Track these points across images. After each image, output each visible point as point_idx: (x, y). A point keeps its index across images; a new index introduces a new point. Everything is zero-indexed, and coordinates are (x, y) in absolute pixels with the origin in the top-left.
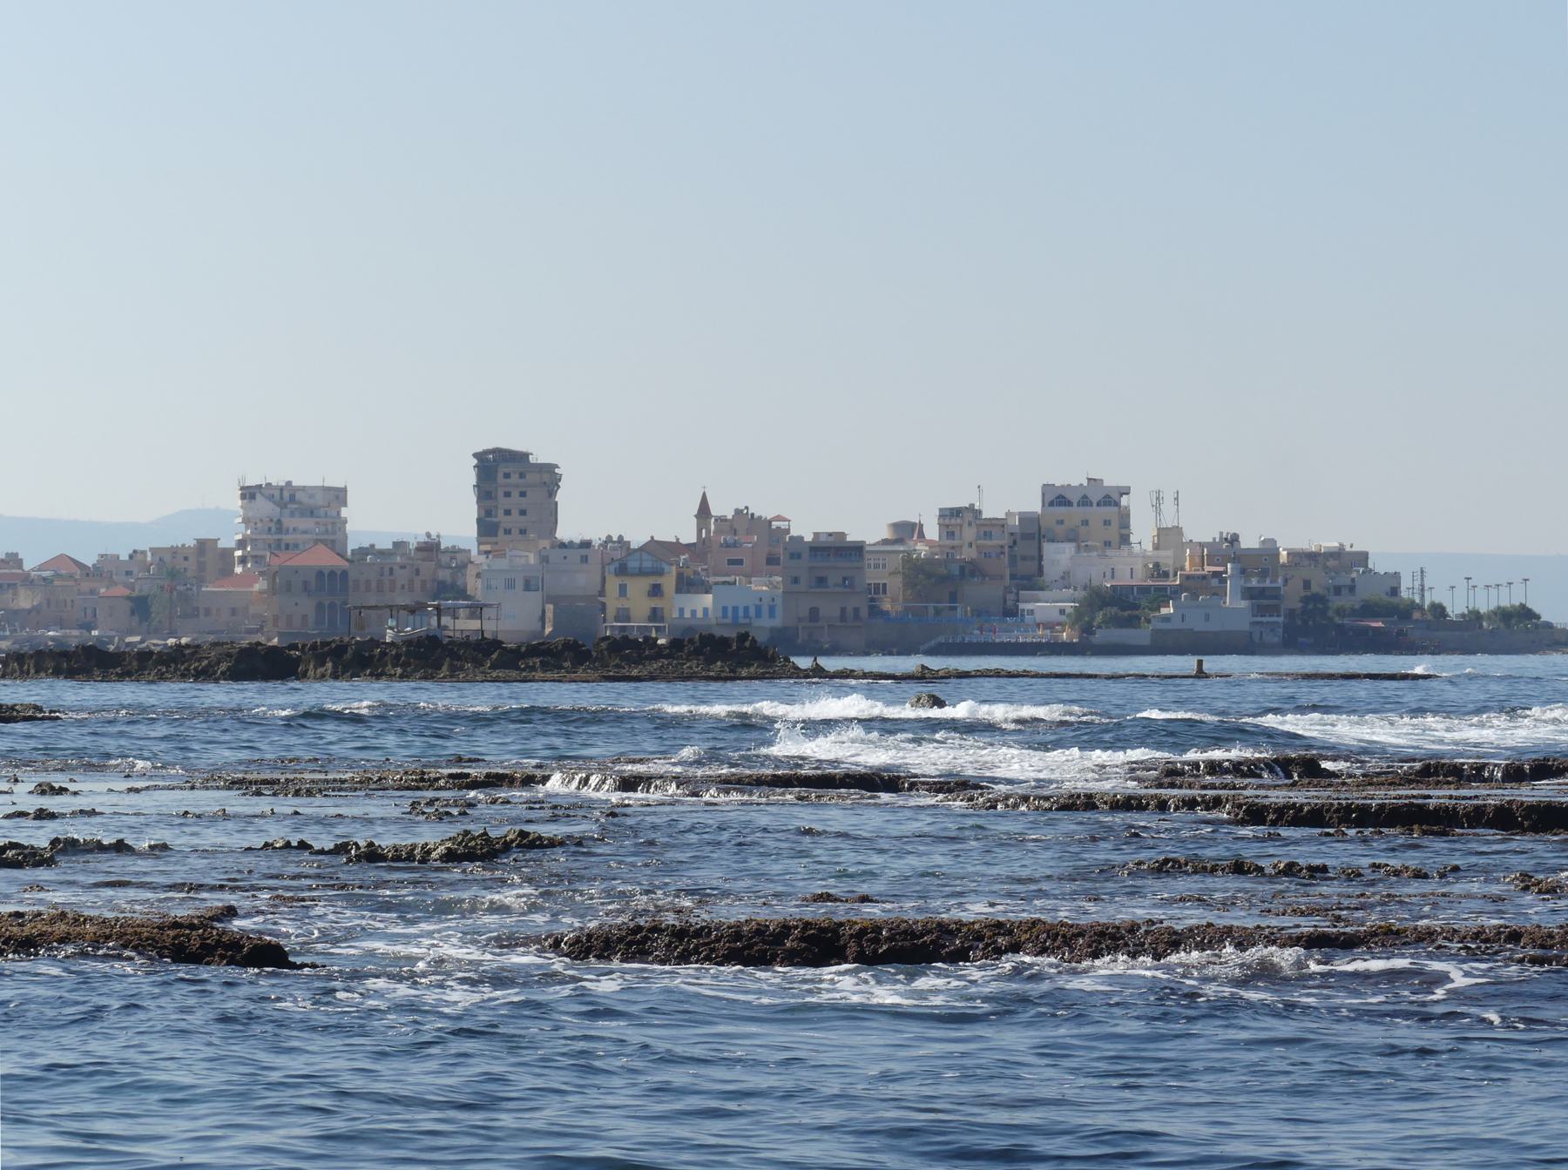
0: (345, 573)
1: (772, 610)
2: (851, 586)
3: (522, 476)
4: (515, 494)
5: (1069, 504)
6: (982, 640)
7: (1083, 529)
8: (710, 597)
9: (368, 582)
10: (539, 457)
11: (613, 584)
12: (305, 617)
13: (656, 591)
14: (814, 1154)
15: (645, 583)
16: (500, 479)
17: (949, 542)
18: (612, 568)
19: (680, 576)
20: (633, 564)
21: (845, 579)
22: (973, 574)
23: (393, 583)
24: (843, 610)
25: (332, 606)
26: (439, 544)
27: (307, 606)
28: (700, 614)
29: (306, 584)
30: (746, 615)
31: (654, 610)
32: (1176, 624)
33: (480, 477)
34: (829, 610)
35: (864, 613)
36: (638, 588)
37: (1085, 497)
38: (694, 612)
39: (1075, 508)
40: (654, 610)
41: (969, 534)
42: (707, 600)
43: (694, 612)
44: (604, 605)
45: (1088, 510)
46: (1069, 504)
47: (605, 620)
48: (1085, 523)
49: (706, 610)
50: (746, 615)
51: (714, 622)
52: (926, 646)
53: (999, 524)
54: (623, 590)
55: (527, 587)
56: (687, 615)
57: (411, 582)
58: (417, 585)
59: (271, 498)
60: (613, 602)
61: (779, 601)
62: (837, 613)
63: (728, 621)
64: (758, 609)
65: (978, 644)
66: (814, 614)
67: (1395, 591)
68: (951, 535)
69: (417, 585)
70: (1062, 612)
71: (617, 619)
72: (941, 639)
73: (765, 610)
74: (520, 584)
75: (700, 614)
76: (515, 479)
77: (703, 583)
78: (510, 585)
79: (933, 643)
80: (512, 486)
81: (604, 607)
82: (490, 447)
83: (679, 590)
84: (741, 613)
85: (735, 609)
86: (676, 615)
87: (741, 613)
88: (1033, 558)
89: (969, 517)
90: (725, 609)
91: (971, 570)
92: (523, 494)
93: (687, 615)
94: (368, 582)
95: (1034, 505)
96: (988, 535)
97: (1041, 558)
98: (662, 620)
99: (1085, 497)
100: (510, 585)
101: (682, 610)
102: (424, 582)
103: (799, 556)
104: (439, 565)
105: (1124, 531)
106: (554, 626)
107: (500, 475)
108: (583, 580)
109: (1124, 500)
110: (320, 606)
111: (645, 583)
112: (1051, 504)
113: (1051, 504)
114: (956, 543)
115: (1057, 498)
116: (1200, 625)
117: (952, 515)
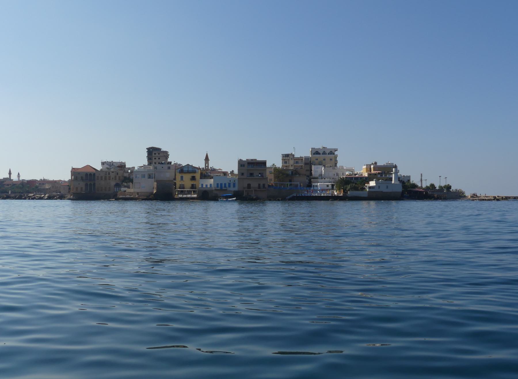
0: (94, 174)
1: (234, 186)
2: (262, 176)
3: (159, 154)
4: (157, 158)
5: (319, 154)
6: (309, 195)
7: (324, 162)
8: (212, 180)
9: (102, 177)
10: (164, 149)
11: (179, 176)
12: (82, 188)
13: (193, 178)
14: (237, 353)
15: (189, 176)
16: (153, 155)
17: (285, 165)
18: (178, 170)
19: (201, 174)
20: (185, 169)
22: (296, 174)
23: (110, 177)
24: (259, 185)
25: (91, 184)
26: (125, 165)
27: (82, 184)
28: (209, 186)
29: (82, 177)
30: (225, 187)
31: (193, 185)
32: (377, 190)
33: (148, 154)
34: (254, 184)
36: (187, 177)
37: (324, 152)
38: (206, 185)
39: (321, 155)
40: (193, 185)
41: (292, 162)
42: (211, 181)
43: (206, 185)
44: (175, 183)
45: (325, 156)
46: (319, 154)
47: (175, 188)
48: (324, 160)
49: (211, 185)
50: (225, 187)
51: (214, 189)
52: (289, 197)
53: (301, 159)
54: (182, 177)
55: (150, 177)
56: (204, 186)
57: (115, 177)
58: (117, 178)
59: (108, 164)
60: (178, 183)
61: (237, 182)
63: (219, 188)
64: (229, 184)
66: (249, 186)
67: (409, 181)
68: (286, 162)
69: (117, 178)
70: (328, 186)
73: (232, 185)
74: (147, 176)
75: (209, 186)
76: (157, 155)
77: (209, 176)
78: (144, 176)
79: (291, 196)
80: (155, 154)
81: (175, 184)
82: (151, 146)
83: (201, 178)
84: (223, 186)
85: (221, 184)
86: (200, 186)
87: (223, 186)
89: (291, 157)
90: (218, 184)
91: (295, 173)
92: (159, 159)
93: (204, 186)
94: (102, 177)
95: (309, 155)
96: (297, 163)
98: (195, 188)
99: (324, 152)
100: (144, 176)
101: (202, 185)
102: (119, 177)
103: (244, 166)
104: (125, 172)
108: (168, 175)
109: (336, 153)
110: (86, 185)
111: (189, 176)
112: (314, 154)
113: (314, 154)
114: (287, 165)
115: (316, 152)
116: (384, 189)
117: (286, 156)
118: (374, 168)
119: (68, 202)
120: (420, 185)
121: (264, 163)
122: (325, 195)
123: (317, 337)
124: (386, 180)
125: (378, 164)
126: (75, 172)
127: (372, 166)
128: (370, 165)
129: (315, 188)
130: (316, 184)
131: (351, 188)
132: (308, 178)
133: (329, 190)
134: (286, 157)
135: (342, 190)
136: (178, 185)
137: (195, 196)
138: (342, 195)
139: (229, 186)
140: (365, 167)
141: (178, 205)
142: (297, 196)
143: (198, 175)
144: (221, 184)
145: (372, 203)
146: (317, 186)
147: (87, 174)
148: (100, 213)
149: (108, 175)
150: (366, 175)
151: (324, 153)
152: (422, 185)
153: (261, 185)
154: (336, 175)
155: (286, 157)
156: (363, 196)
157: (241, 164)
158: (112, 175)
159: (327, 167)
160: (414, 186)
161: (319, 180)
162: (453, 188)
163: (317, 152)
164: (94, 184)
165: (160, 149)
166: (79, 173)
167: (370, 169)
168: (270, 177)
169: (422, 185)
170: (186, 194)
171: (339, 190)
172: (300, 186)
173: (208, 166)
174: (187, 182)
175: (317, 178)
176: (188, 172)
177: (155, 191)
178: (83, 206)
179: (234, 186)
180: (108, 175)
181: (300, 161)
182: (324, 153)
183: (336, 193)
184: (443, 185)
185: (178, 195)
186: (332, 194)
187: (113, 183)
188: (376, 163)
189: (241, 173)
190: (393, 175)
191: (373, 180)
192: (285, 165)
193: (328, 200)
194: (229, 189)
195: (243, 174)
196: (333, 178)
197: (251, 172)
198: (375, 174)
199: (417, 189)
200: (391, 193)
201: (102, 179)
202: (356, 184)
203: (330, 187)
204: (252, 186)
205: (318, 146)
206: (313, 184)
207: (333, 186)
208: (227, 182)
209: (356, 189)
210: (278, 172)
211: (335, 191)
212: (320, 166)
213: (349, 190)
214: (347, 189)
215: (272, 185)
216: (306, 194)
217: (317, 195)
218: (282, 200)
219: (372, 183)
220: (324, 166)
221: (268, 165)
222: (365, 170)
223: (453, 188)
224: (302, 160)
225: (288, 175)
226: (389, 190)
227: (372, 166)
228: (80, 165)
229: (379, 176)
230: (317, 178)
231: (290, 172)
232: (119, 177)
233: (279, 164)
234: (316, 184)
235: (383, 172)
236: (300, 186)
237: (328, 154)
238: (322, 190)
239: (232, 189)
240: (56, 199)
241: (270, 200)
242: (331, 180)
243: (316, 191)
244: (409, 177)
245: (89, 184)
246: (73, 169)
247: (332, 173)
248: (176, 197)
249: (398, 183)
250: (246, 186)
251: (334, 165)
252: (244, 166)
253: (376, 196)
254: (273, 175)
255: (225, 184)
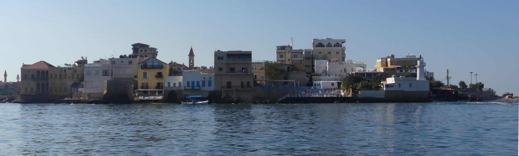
1: (210, 85)
2: (246, 72)
3: (145, 51)
5: (323, 46)
6: (307, 96)
9: (56, 75)
10: (152, 46)
12: (32, 89)
13: (160, 75)
15: (154, 72)
16: (139, 52)
19: (171, 70)
21: (243, 69)
22: (293, 70)
23: (66, 75)
24: (242, 83)
25: (43, 84)
27: (33, 84)
28: (177, 85)
29: (32, 76)
34: (236, 83)
35: (252, 84)
36: (152, 74)
37: (329, 43)
38: (175, 84)
40: (159, 84)
41: (289, 56)
42: (180, 78)
43: (175, 84)
45: (331, 48)
46: (323, 46)
48: (330, 53)
49: (180, 83)
52: (281, 99)
53: (300, 52)
54: (145, 74)
55: (105, 73)
56: (172, 85)
57: (73, 75)
58: (75, 76)
60: (141, 81)
61: (213, 79)
62: (240, 84)
63: (190, 88)
64: (204, 82)
65: (305, 98)
66: (229, 84)
68: (281, 56)
69: (75, 76)
70: (333, 84)
71: (142, 88)
72: (288, 96)
74: (101, 73)
75: (177, 85)
76: (143, 52)
79: (284, 98)
84: (196, 84)
86: (166, 85)
87: (196, 84)
88: (309, 66)
89: (288, 49)
90: (188, 83)
91: (292, 68)
93: (172, 85)
94: (56, 75)
95: (310, 47)
96: (295, 56)
97: (313, 66)
98: (162, 88)
99: (329, 43)
101: (169, 83)
102: (78, 75)
103: (222, 58)
105: (344, 56)
106: (108, 90)
107: (139, 51)
109: (344, 45)
110: (38, 85)
111: (154, 72)
112: (317, 46)
113: (317, 46)
114: (283, 59)
115: (319, 44)
116: (406, 88)
117: (281, 49)
118: (390, 61)
119: (17, 107)
120: (446, 84)
121: (248, 55)
122: (329, 96)
123: (365, 146)
124: (407, 76)
125: (395, 57)
126: (26, 70)
127: (389, 60)
128: (386, 59)
129: (318, 87)
130: (318, 82)
131: (363, 88)
132: (309, 75)
133: (334, 89)
134: (282, 50)
135: (351, 90)
136: (140, 85)
137: (160, 98)
138: (350, 95)
139: (204, 85)
140: (380, 60)
141: (139, 108)
142: (291, 98)
143: (166, 72)
144: (193, 83)
145: (391, 107)
146: (319, 85)
147: (38, 72)
148: (59, 119)
149: (63, 73)
150: (381, 70)
151: (329, 45)
152: (448, 83)
153: (245, 83)
154: (343, 71)
155: (282, 50)
156: (378, 97)
157: (219, 56)
158: (69, 73)
159: (333, 61)
160: (440, 84)
161: (322, 77)
162: (486, 88)
163: (320, 43)
164: (47, 84)
165: (148, 46)
166: (29, 71)
167: (387, 62)
168: (260, 75)
169: (448, 83)
170: (149, 96)
171: (347, 89)
172: (297, 85)
173: (193, 63)
174: (152, 81)
175: (320, 75)
176: (153, 67)
177: (105, 92)
178: (34, 109)
179: (210, 85)
180: (63, 73)
181: (298, 55)
182: (329, 45)
183: (343, 94)
184: (474, 83)
185: (138, 96)
186: (338, 95)
187: (69, 83)
188: (393, 56)
189: (218, 67)
190: (418, 69)
191: (390, 77)
192: (281, 59)
193: (333, 102)
194: (203, 89)
195: (221, 69)
196: (340, 75)
197: (232, 66)
198: (393, 69)
199: (442, 88)
200: (415, 92)
201: (56, 78)
202: (369, 81)
203: (336, 85)
204: (232, 84)
205: (322, 36)
206: (315, 82)
207: (339, 84)
208: (200, 80)
209: (368, 87)
210: (269, 66)
211: (342, 91)
212: (324, 61)
213: (360, 90)
214: (358, 88)
215: (414, 112)
216: (303, 94)
217: (317, 96)
218: (270, 103)
219: (391, 81)
220: (330, 61)
221: (255, 59)
222: (380, 65)
223: (486, 88)
224: (302, 53)
225: (282, 71)
226: (414, 89)
227: (389, 60)
228: (31, 61)
229: (398, 71)
230: (320, 75)
231: (286, 68)
232: (78, 75)
233: (273, 58)
234: (318, 82)
235: (405, 67)
236: (297, 85)
237: (334, 46)
238: (326, 90)
239: (207, 88)
240: (5, 102)
241: (255, 103)
242: (337, 77)
243: (317, 91)
244: (432, 74)
245: (45, 83)
246: (24, 65)
247: (338, 68)
248: (136, 99)
249: (424, 79)
250: (225, 84)
251: (341, 59)
252: (222, 58)
253: (394, 97)
254: (264, 71)
255: (198, 82)
